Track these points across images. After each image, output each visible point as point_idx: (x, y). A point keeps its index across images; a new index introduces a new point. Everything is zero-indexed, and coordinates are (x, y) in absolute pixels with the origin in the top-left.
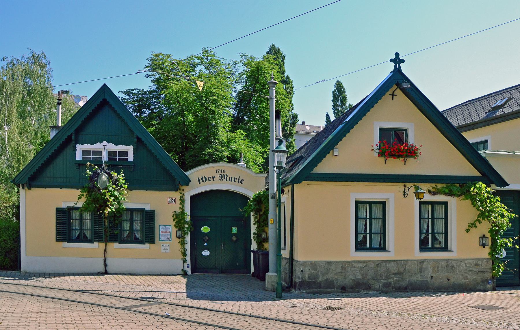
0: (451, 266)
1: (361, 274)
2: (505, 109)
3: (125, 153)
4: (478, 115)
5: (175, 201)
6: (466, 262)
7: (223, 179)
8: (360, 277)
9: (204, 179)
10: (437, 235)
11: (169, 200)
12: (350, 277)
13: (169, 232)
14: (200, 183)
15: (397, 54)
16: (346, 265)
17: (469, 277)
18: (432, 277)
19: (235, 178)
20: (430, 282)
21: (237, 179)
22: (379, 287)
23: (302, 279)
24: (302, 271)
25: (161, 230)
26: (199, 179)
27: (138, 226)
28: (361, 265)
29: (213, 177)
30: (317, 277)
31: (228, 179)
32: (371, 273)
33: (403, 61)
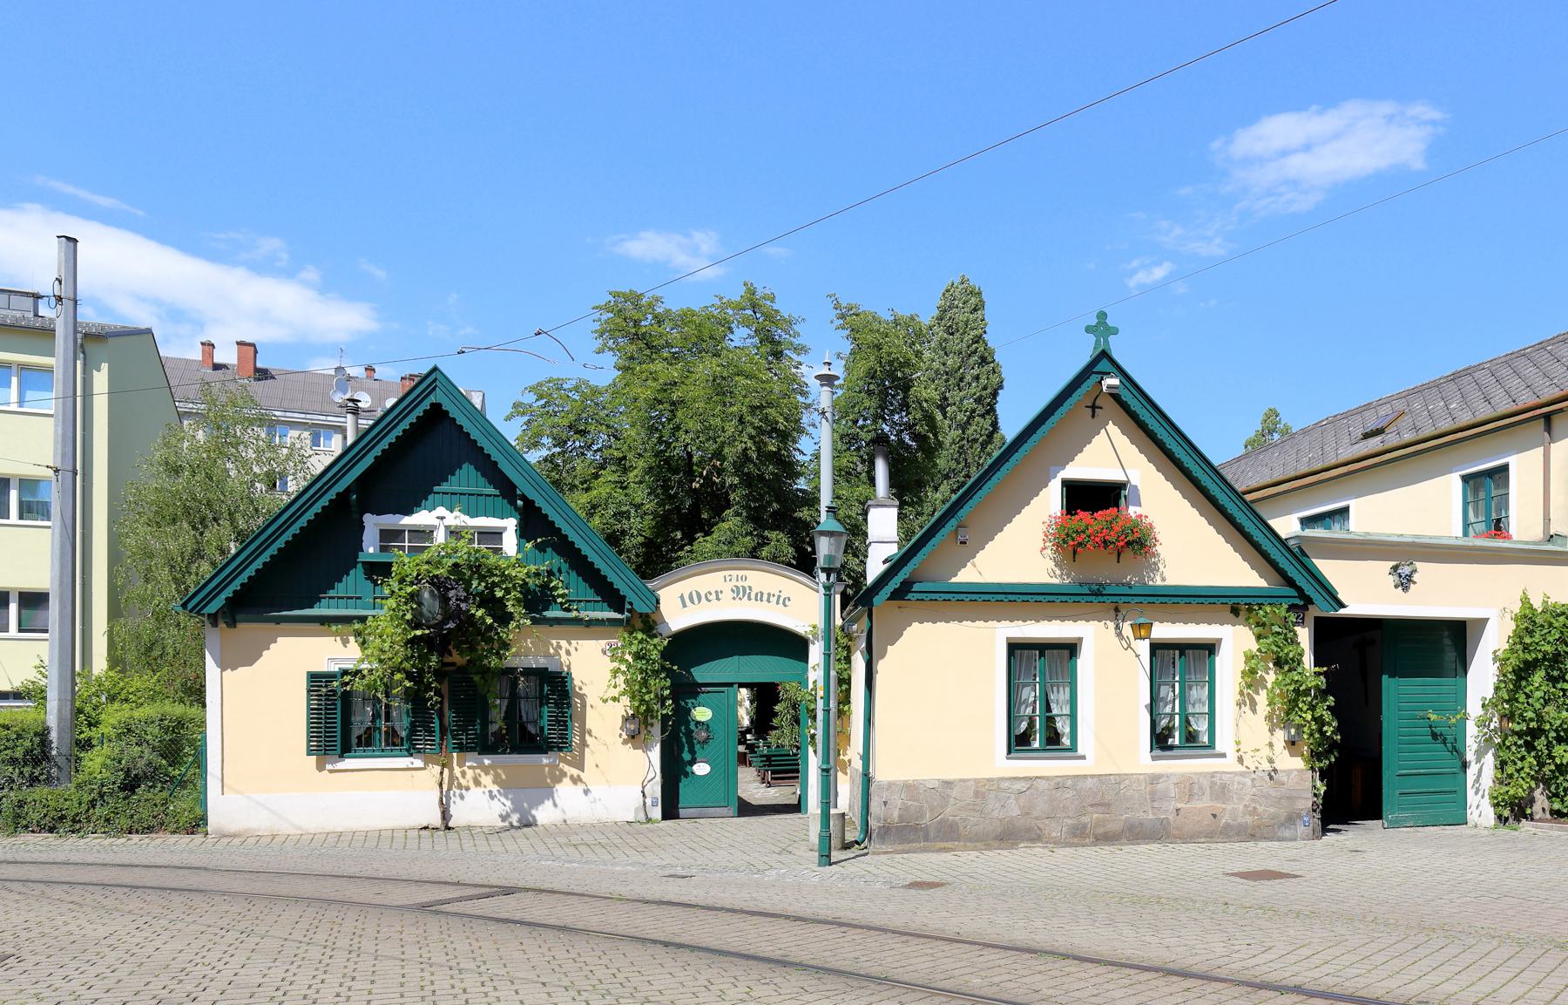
0: (1220, 789)
1: (1019, 806)
2: (1389, 436)
3: (496, 535)
4: (1398, 433)
7: (741, 595)
8: (1016, 812)
12: (995, 814)
14: (684, 605)
15: (1102, 316)
16: (984, 790)
17: (1260, 809)
18: (1178, 810)
20: (1174, 821)
22: (1059, 834)
24: (885, 803)
26: (682, 597)
29: (716, 592)
30: (921, 815)
31: (753, 596)
32: (1041, 807)
33: (1115, 331)
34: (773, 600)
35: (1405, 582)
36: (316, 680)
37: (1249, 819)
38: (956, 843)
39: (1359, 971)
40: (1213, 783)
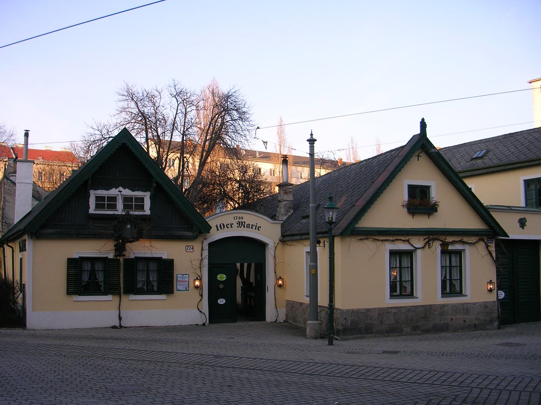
0: (466, 308)
5: (193, 249)
6: (477, 304)
7: (241, 226)
9: (222, 226)
10: (453, 281)
11: (187, 248)
13: (186, 281)
14: (218, 230)
16: (383, 312)
17: (480, 317)
19: (252, 225)
21: (254, 226)
23: (345, 326)
24: (345, 319)
25: (179, 279)
26: (217, 226)
27: (153, 277)
28: (394, 311)
29: (231, 224)
31: (246, 226)
34: (254, 227)
35: (522, 223)
36: (72, 262)
37: (477, 322)
38: (372, 335)
39: (329, 372)
40: (464, 308)
